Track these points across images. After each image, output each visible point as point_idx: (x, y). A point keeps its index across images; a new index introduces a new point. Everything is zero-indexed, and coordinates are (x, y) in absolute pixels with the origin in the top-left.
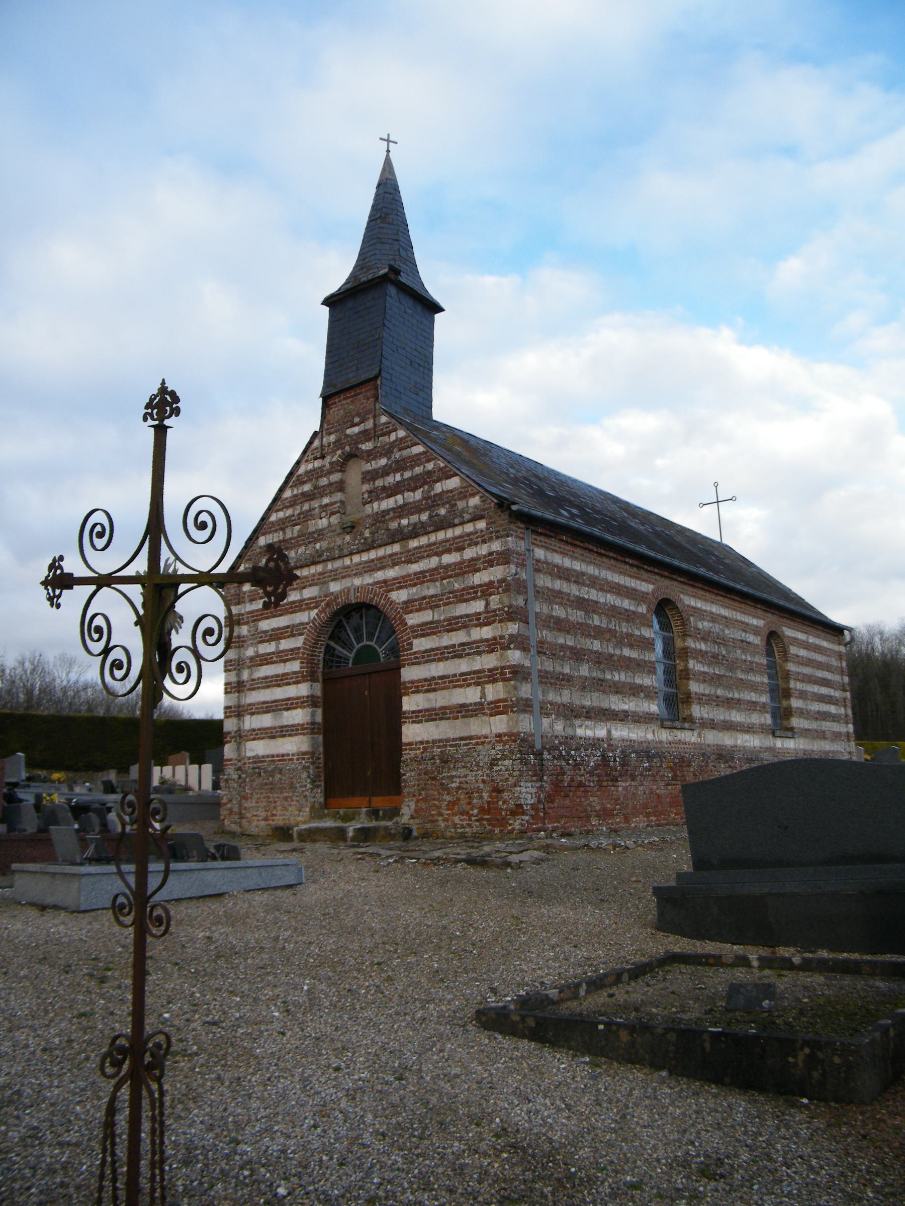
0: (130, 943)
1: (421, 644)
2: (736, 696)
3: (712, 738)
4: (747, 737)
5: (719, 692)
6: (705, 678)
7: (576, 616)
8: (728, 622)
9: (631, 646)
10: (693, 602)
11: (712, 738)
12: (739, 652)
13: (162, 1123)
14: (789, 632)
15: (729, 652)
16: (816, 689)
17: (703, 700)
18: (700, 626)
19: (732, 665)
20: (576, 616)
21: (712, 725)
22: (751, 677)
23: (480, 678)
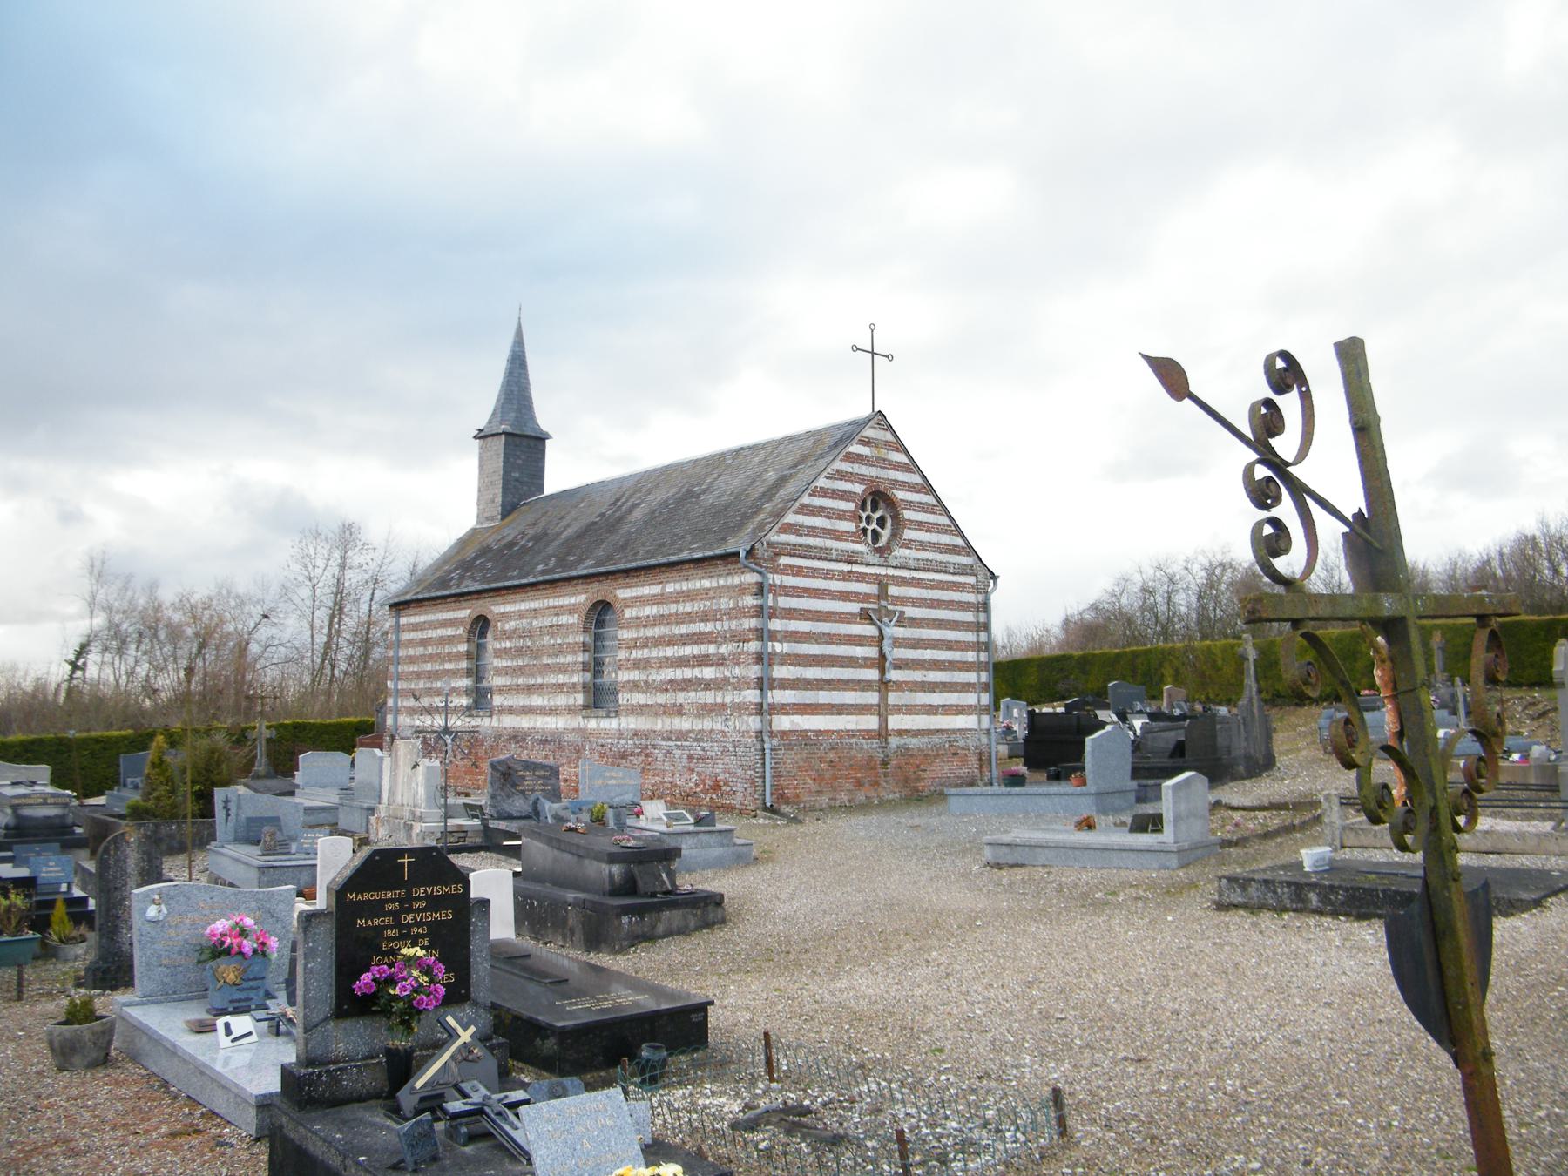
0: (214, 1060)
1: (460, 631)
2: (540, 681)
3: (509, 722)
4: (548, 719)
5: (520, 681)
6: (506, 671)
7: (420, 651)
8: (535, 612)
9: (450, 661)
10: (502, 609)
11: (509, 722)
12: (546, 638)
13: (341, 609)
14: (624, 593)
15: (534, 642)
16: (656, 653)
17: (502, 690)
18: (507, 627)
19: (536, 654)
20: (420, 651)
21: (511, 711)
22: (561, 660)
23: (915, 622)
